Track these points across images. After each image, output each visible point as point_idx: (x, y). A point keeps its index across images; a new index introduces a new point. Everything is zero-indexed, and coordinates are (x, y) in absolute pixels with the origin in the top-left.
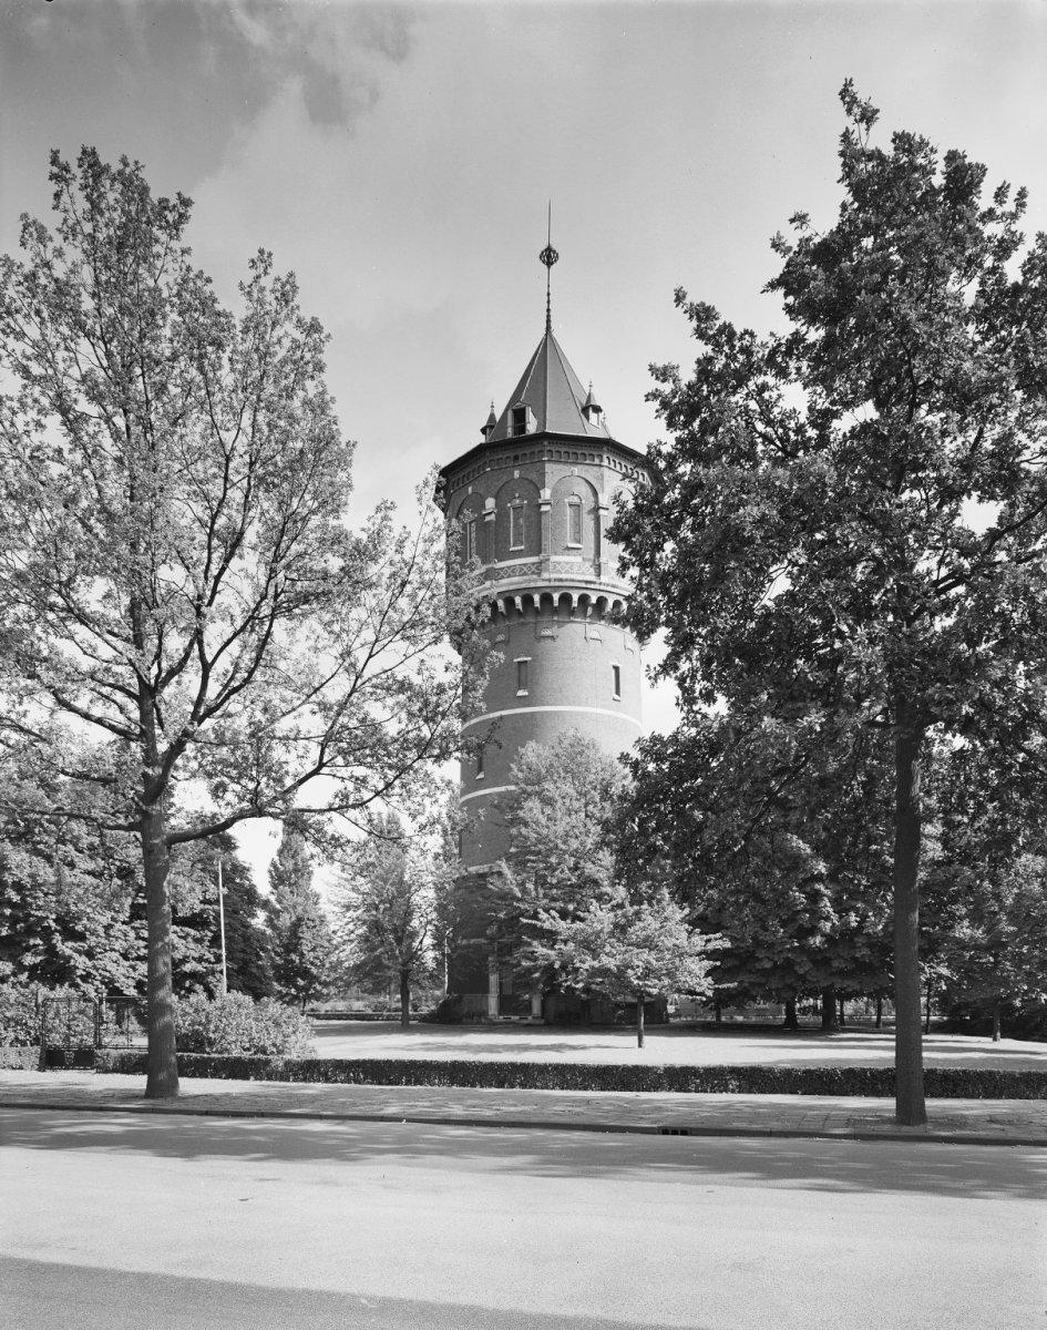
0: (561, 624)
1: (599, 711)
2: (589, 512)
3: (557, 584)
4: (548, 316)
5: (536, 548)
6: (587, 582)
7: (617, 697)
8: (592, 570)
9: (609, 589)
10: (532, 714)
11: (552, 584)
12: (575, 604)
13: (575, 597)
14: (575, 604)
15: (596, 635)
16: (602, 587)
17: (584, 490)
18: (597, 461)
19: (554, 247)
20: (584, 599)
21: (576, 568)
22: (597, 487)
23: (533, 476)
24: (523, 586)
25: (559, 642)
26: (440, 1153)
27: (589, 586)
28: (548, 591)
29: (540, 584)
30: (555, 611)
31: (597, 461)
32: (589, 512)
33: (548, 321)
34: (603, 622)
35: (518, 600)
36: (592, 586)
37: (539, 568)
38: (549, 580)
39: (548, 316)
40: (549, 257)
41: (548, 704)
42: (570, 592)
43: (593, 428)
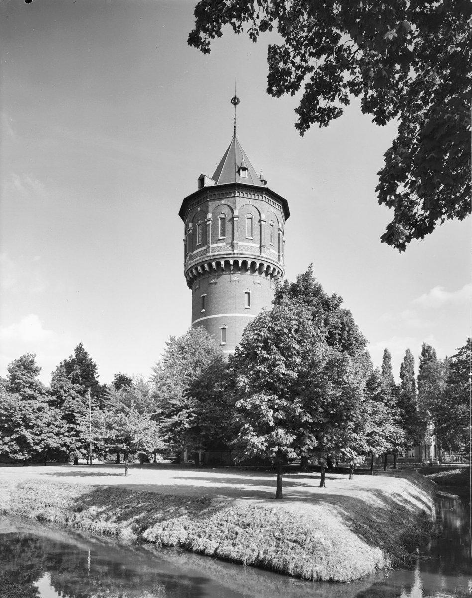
0: (218, 277)
1: (236, 315)
2: (229, 221)
3: (213, 257)
4: (235, 129)
5: (205, 242)
6: (227, 254)
7: (249, 307)
8: (230, 248)
9: (239, 255)
10: (207, 320)
11: (211, 258)
12: (240, 265)
13: (240, 262)
14: (240, 265)
15: (236, 279)
16: (235, 255)
17: (226, 210)
18: (232, 195)
19: (237, 96)
20: (227, 263)
21: (222, 248)
22: (233, 207)
23: (204, 209)
24: (200, 261)
25: (218, 285)
26: (305, 500)
27: (228, 256)
28: (210, 261)
29: (206, 259)
30: (239, 269)
31: (232, 195)
32: (229, 221)
33: (234, 132)
34: (240, 272)
35: (214, 264)
36: (230, 256)
37: (206, 251)
38: (209, 256)
39: (235, 129)
40: (235, 101)
41: (210, 315)
42: (219, 260)
43: (244, 178)
